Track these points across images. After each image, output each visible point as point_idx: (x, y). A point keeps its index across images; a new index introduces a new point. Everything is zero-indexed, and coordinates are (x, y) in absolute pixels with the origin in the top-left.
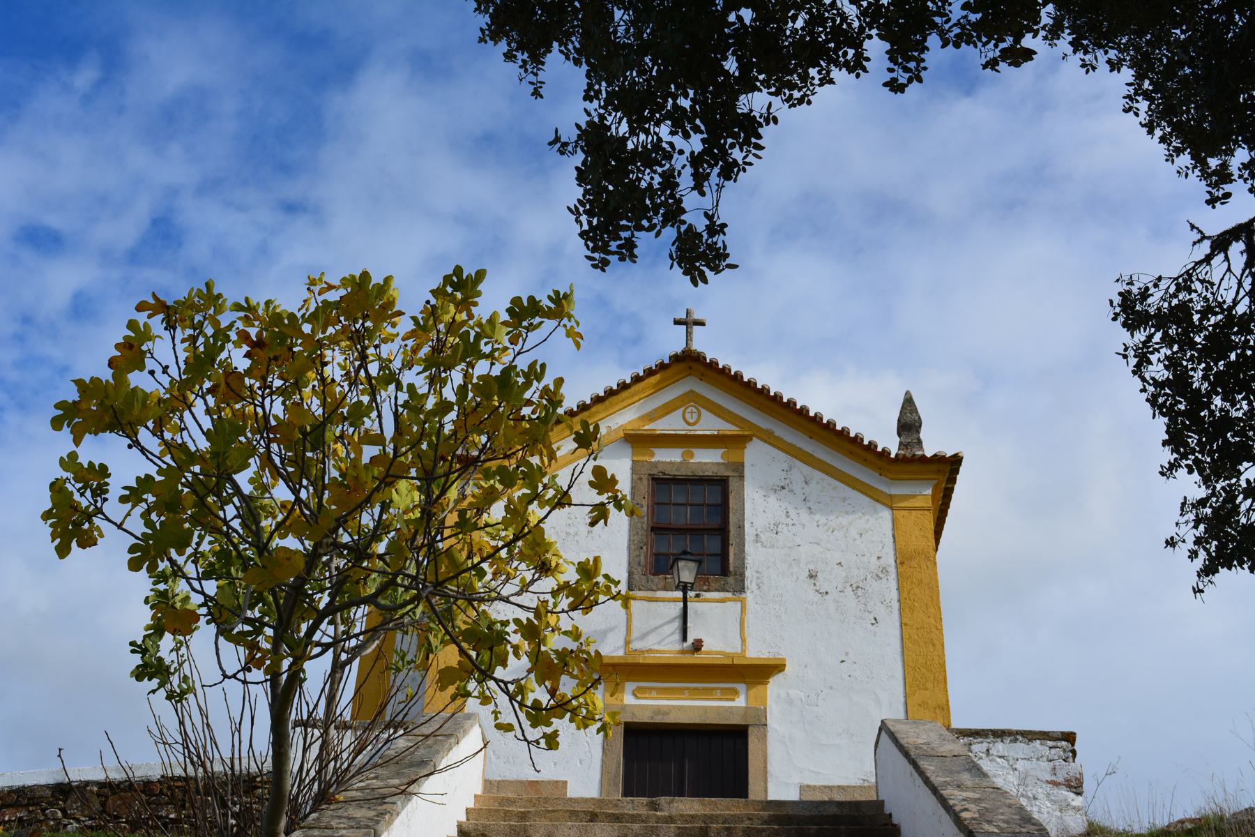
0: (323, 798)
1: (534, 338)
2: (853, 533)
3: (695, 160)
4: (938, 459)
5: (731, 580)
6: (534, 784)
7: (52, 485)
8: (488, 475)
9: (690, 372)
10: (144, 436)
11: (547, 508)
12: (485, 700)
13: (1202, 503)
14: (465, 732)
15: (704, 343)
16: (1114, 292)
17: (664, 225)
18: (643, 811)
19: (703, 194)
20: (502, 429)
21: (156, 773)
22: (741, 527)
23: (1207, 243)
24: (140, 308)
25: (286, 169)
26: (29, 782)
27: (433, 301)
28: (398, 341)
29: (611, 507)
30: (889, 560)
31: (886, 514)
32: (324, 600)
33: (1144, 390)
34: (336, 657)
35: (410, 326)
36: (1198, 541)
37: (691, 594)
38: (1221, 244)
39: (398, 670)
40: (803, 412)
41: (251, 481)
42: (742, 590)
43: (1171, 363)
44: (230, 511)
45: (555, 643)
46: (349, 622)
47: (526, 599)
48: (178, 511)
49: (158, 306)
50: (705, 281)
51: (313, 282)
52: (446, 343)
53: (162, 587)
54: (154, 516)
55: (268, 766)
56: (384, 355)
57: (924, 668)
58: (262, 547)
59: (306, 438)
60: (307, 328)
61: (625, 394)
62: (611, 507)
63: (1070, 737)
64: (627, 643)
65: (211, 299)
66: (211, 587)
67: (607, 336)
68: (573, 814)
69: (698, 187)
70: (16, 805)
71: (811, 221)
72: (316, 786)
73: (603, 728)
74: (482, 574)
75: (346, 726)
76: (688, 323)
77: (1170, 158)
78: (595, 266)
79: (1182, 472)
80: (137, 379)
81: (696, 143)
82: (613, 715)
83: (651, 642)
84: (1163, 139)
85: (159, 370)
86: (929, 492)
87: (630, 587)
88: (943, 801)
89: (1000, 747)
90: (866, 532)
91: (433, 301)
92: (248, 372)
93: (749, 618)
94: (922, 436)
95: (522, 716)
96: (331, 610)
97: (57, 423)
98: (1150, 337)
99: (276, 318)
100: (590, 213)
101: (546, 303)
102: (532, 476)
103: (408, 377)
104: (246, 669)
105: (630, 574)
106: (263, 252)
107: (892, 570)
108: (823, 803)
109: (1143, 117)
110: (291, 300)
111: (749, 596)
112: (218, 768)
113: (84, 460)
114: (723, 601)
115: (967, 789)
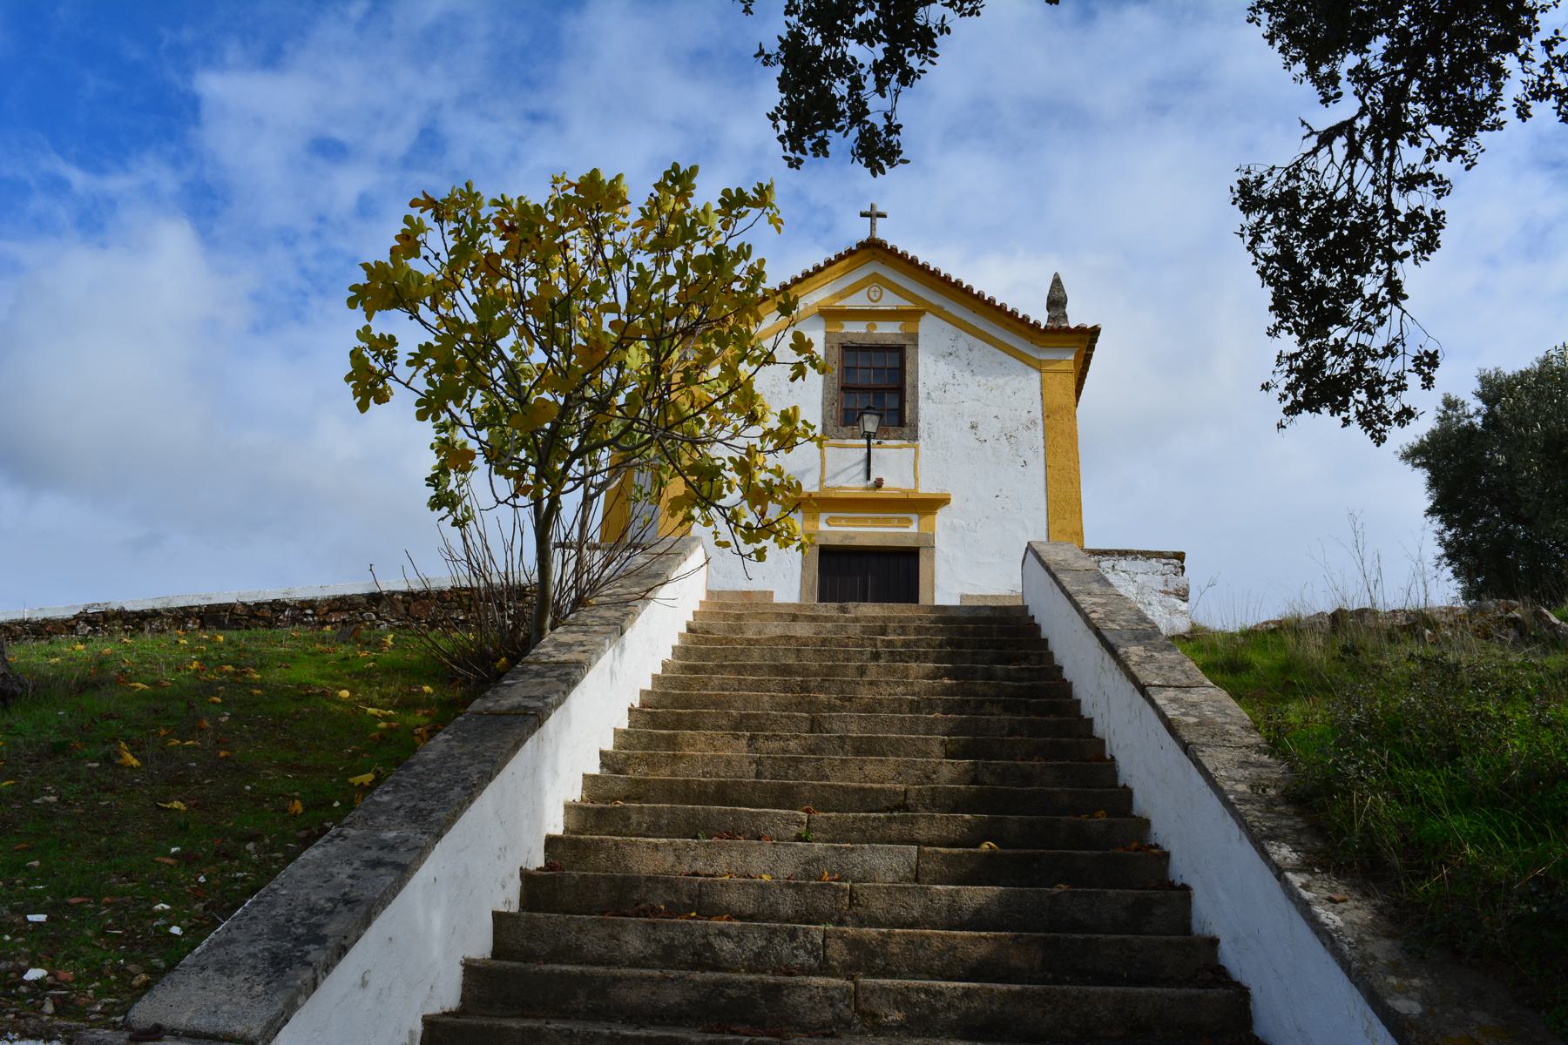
0: (579, 602)
1: (742, 224)
2: (1008, 391)
3: (877, 67)
4: (1081, 330)
5: (906, 430)
6: (747, 594)
7: (352, 353)
8: (704, 340)
9: (873, 257)
10: (424, 311)
11: (755, 366)
12: (709, 522)
13: (1296, 356)
14: (691, 551)
15: (886, 232)
16: (1233, 180)
17: (851, 124)
18: (835, 614)
19: (883, 96)
20: (714, 302)
21: (447, 585)
22: (915, 387)
23: (1315, 138)
24: (413, 204)
25: (530, 84)
26: (349, 591)
27: (656, 194)
28: (629, 229)
29: (807, 365)
30: (1037, 413)
31: (1036, 376)
32: (574, 444)
33: (1255, 263)
34: (586, 491)
35: (639, 216)
36: (1290, 388)
37: (874, 442)
38: (1326, 138)
39: (637, 501)
40: (969, 290)
41: (512, 349)
42: (916, 438)
43: (1280, 241)
44: (496, 373)
45: (761, 477)
46: (595, 463)
47: (739, 441)
48: (455, 368)
49: (429, 203)
50: (883, 172)
51: (556, 181)
52: (670, 227)
53: (443, 435)
54: (435, 377)
55: (535, 578)
56: (618, 241)
57: (1064, 501)
58: (522, 401)
59: (553, 314)
60: (551, 218)
61: (819, 276)
62: (807, 365)
63: (1180, 556)
64: (821, 481)
65: (470, 197)
66: (484, 435)
67: (800, 228)
68: (779, 616)
69: (880, 90)
70: (339, 610)
71: (978, 124)
72: (573, 595)
73: (801, 547)
74: (701, 423)
75: (595, 547)
76: (872, 215)
77: (1287, 66)
78: (791, 166)
79: (1284, 333)
80: (415, 264)
81: (879, 51)
82: (809, 536)
83: (840, 481)
84: (1282, 50)
85: (432, 257)
86: (1072, 357)
87: (824, 431)
88: (1076, 605)
89: (1123, 564)
90: (1019, 391)
91: (656, 194)
92: (504, 254)
93: (922, 461)
94: (1068, 310)
95: (738, 537)
96: (579, 453)
97: (352, 303)
98: (1263, 219)
99: (524, 208)
100: (788, 119)
101: (751, 194)
102: (743, 339)
103: (637, 259)
104: (515, 496)
105: (824, 425)
106: (514, 157)
107: (1040, 422)
108: (979, 607)
109: (1264, 29)
110: (539, 195)
111: (921, 443)
112: (496, 580)
113: (376, 332)
114: (900, 447)
115: (1096, 595)
